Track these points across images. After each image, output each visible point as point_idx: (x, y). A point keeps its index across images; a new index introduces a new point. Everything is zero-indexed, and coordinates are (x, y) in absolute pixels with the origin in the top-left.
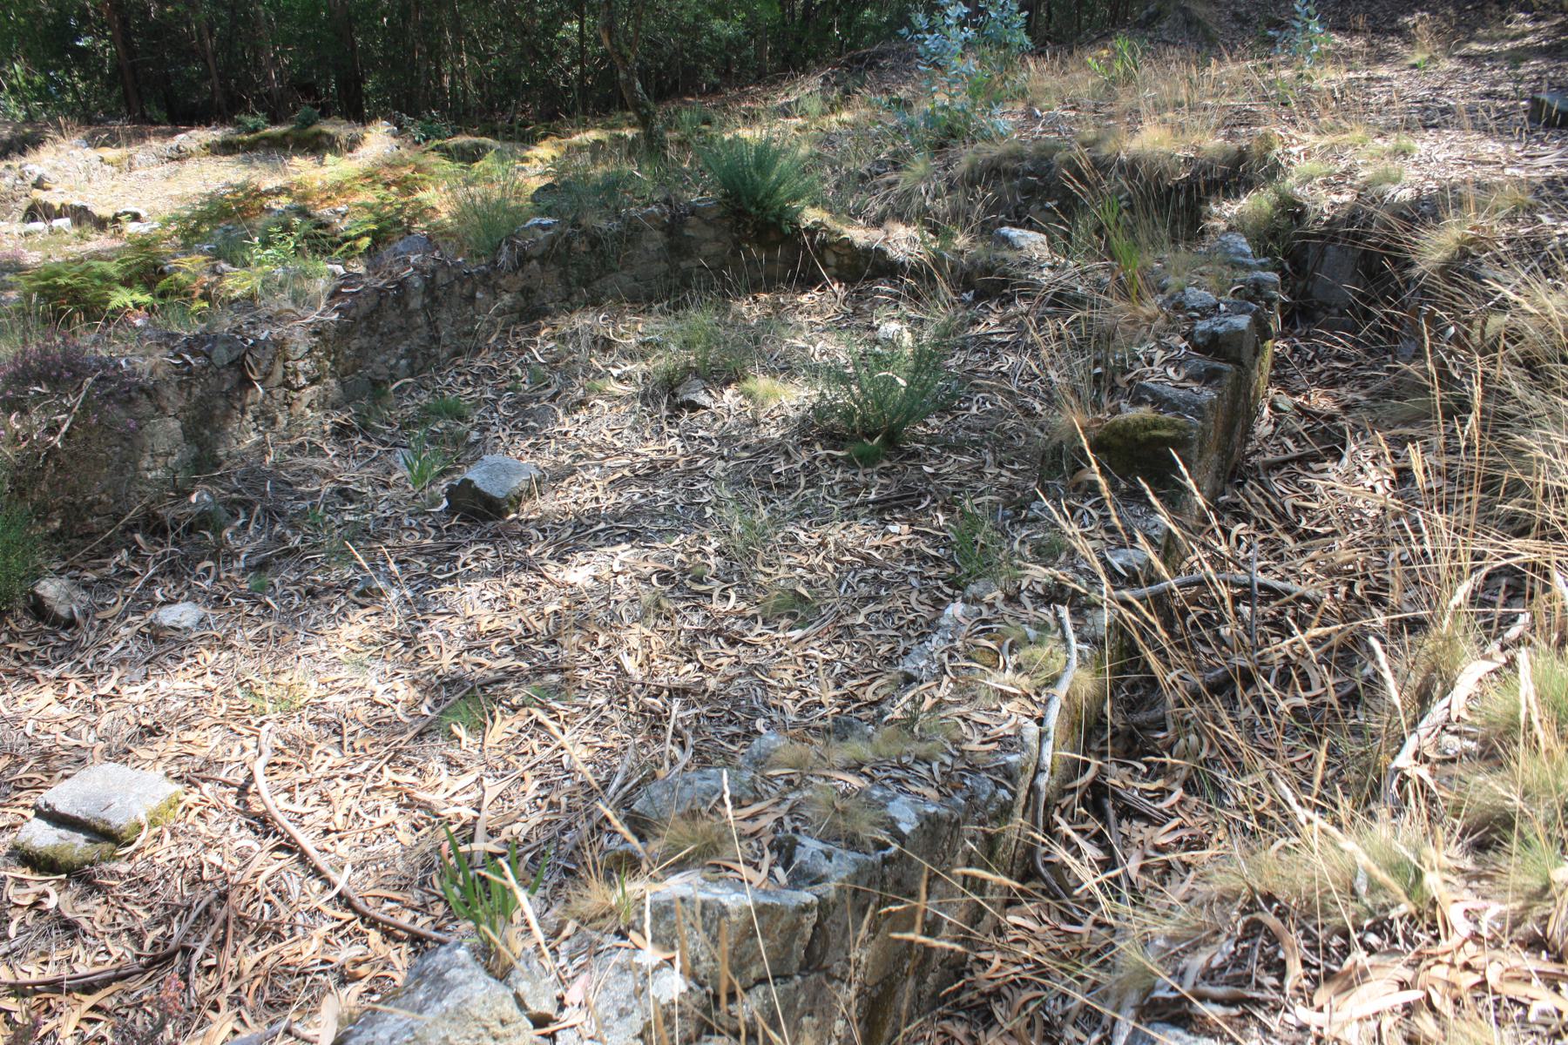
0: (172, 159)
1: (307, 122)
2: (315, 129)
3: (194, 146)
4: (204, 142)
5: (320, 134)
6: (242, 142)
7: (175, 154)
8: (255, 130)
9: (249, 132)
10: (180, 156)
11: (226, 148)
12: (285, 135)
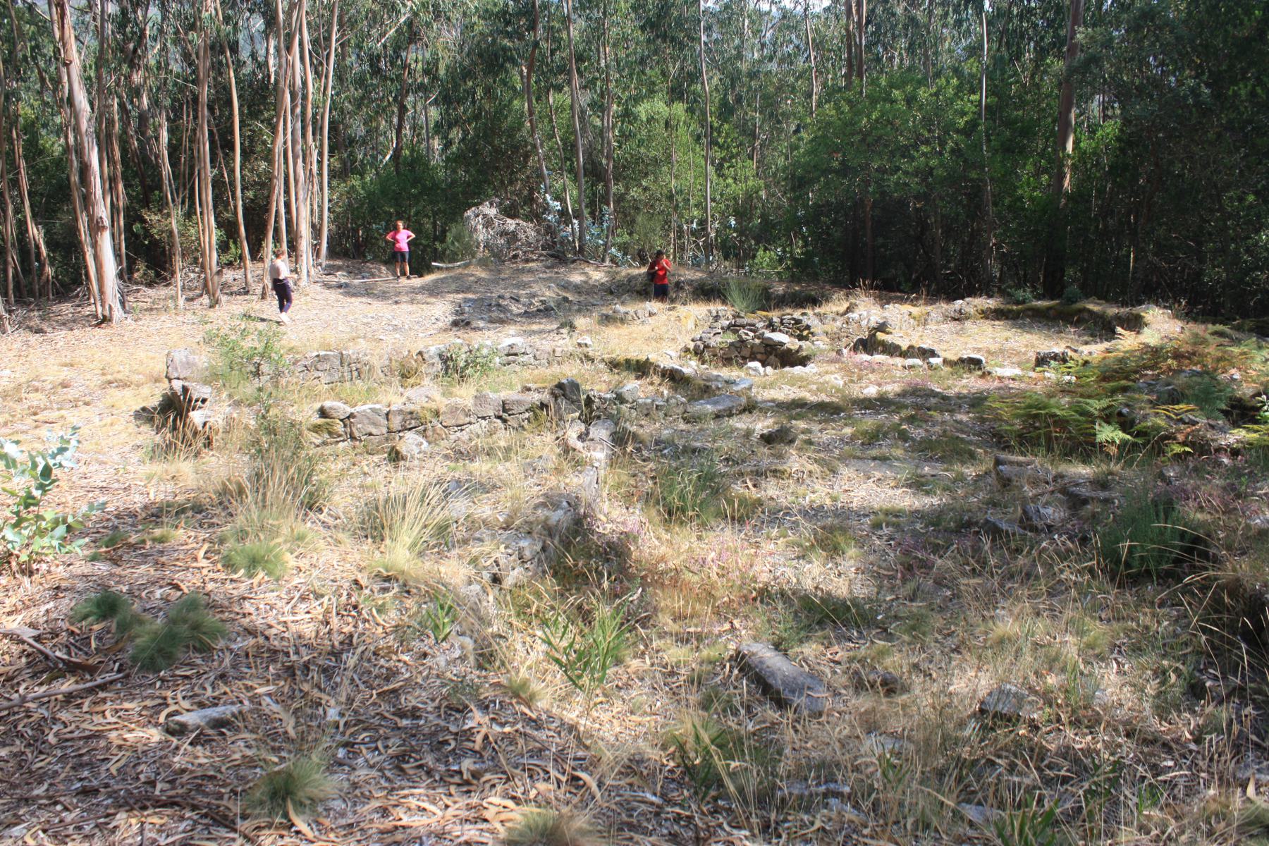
0: (954, 319)
1: (1071, 301)
2: (1079, 305)
3: (972, 311)
4: (979, 308)
5: (1085, 310)
6: (1010, 311)
7: (957, 316)
8: (1023, 302)
9: (1017, 303)
10: (960, 317)
11: (998, 314)
12: (1049, 308)
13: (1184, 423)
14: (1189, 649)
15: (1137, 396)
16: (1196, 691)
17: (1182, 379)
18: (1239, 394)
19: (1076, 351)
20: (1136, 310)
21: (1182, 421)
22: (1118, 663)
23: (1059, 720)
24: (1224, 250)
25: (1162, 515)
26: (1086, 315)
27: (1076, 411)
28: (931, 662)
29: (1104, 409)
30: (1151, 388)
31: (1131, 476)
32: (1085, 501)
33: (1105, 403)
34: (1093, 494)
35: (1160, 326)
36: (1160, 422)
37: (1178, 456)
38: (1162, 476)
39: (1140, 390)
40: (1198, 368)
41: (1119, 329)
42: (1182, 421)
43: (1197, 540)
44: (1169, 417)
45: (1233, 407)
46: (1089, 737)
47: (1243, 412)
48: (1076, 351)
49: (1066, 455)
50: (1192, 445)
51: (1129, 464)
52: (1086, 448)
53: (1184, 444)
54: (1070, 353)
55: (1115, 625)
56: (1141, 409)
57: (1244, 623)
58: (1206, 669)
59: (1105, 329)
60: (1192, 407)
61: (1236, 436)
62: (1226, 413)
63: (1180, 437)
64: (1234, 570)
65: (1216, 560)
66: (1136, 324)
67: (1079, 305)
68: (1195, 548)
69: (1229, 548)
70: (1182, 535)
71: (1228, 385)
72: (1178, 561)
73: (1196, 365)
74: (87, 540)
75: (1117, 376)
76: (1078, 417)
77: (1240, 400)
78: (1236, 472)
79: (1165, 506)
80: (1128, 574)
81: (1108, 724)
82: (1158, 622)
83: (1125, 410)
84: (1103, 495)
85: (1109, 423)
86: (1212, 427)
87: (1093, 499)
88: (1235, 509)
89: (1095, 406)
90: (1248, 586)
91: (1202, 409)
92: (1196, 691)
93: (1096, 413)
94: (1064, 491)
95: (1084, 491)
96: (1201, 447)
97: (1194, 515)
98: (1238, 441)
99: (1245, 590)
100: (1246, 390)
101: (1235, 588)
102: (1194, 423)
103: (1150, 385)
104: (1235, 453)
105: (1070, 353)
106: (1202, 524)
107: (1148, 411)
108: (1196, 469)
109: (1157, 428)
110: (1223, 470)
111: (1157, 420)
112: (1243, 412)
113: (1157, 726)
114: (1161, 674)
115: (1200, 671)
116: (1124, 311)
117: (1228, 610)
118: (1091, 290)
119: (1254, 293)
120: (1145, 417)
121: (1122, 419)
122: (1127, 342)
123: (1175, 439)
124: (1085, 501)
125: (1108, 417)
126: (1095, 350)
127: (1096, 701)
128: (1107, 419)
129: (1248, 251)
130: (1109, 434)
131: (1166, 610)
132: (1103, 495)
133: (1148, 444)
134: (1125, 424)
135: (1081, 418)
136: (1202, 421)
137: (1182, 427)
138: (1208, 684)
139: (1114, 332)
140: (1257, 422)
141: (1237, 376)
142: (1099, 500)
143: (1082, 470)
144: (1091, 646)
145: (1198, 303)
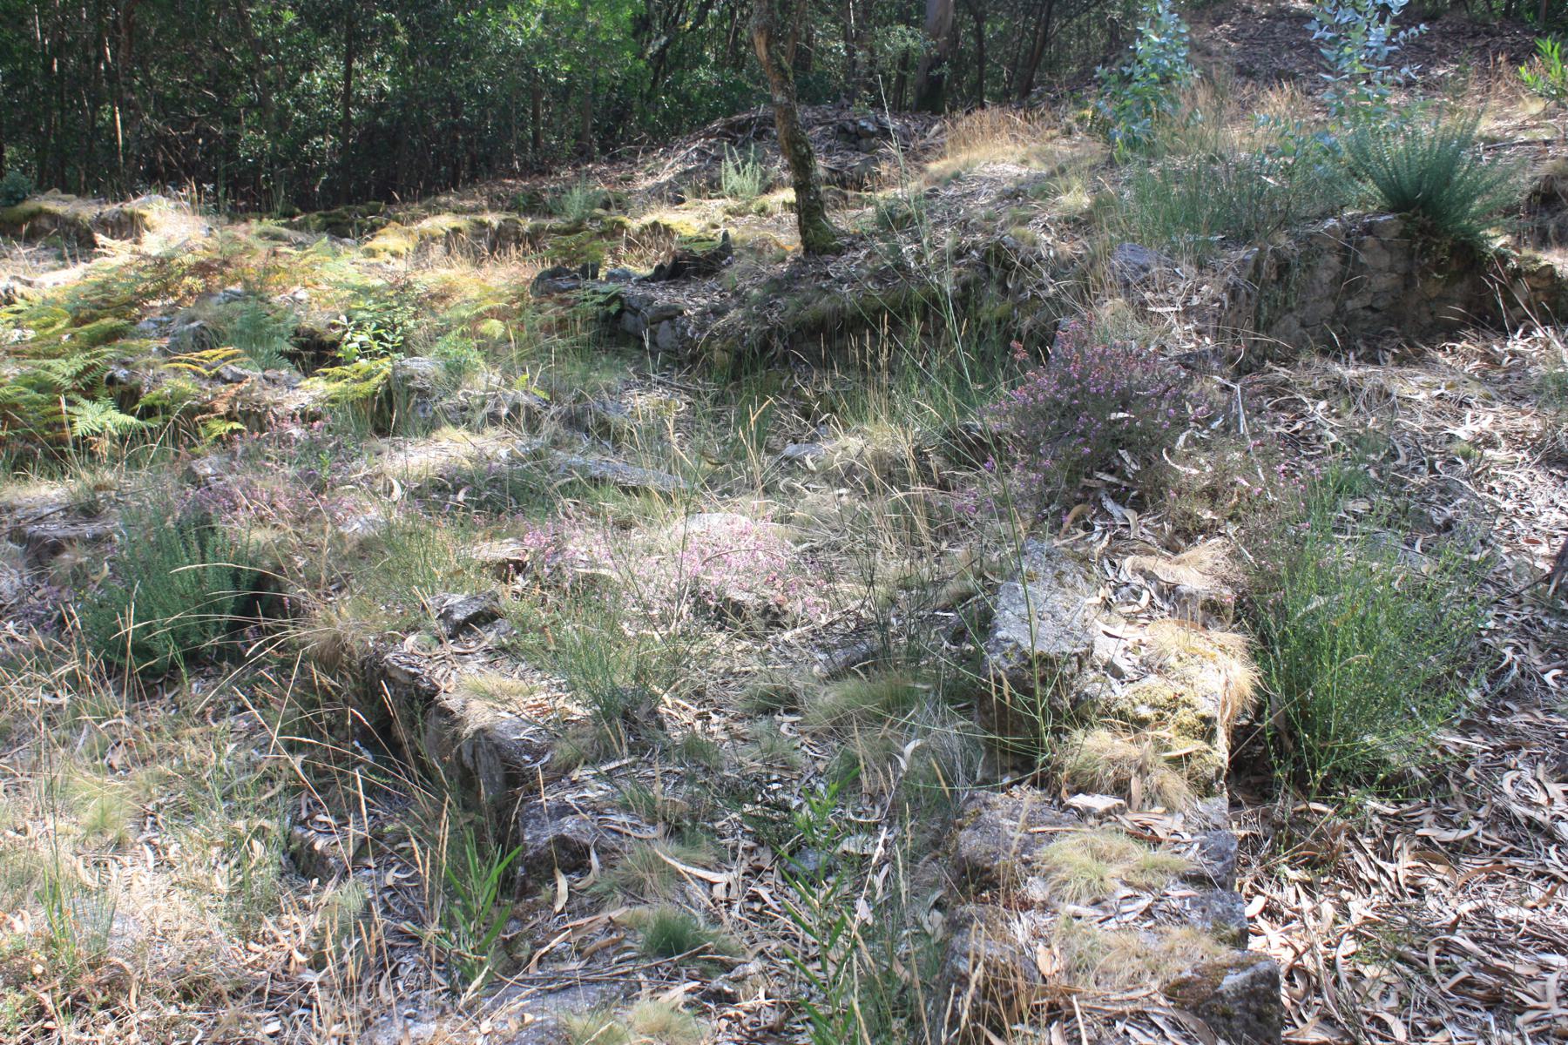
2: (32, 204)
5: (41, 213)
13: (226, 381)
14: (280, 786)
15: (135, 343)
16: (303, 864)
17: (213, 307)
18: (307, 324)
19: (29, 284)
20: (133, 205)
21: (218, 377)
22: (155, 848)
23: (41, 1012)
24: (262, 105)
25: (196, 547)
26: (45, 223)
27: (30, 386)
28: (759, 870)
29: (79, 375)
30: (162, 329)
31: (144, 489)
32: (56, 548)
33: (78, 362)
34: (70, 532)
35: (172, 225)
36: (186, 385)
37: (223, 442)
38: (192, 478)
39: (144, 334)
40: (237, 288)
41: (100, 238)
42: (218, 377)
43: (261, 581)
44: (197, 374)
45: (305, 346)
46: (112, 1026)
47: (315, 352)
48: (29, 284)
49: (14, 468)
50: (246, 417)
51: (134, 463)
52: (52, 450)
53: (229, 417)
54: (20, 288)
55: (139, 774)
56: (148, 366)
57: (356, 719)
58: (311, 817)
59: (77, 241)
60: (231, 350)
61: (313, 390)
62: (292, 357)
63: (222, 408)
64: (329, 622)
65: (297, 611)
66: (128, 227)
67: (32, 204)
68: (261, 595)
69: (314, 583)
70: (236, 577)
71: (288, 311)
72: (234, 628)
73: (233, 282)
74: (534, 989)
75: (105, 318)
76: (32, 394)
77: (312, 333)
78: (313, 447)
79: (201, 528)
80: (148, 674)
81: (143, 984)
82: (217, 749)
83: (121, 373)
84: (88, 530)
85: (94, 399)
86: (274, 382)
87: (70, 540)
88: (317, 511)
89: (63, 370)
90: (356, 645)
91: (252, 354)
92: (303, 864)
93: (68, 384)
94: (17, 536)
95: (55, 529)
96: (255, 418)
97: (252, 534)
98: (315, 400)
99: (351, 654)
100: (315, 319)
101: (332, 658)
102: (239, 379)
103: (160, 323)
104: (308, 417)
105: (20, 288)
106: (264, 550)
107: (163, 368)
108: (248, 456)
109: (178, 396)
110: (293, 450)
111: (174, 381)
112: (315, 352)
113: (233, 957)
114: (233, 845)
115: (303, 823)
116: (110, 209)
117: (330, 698)
118: (56, 178)
119: (321, 169)
120: (157, 380)
121: (117, 390)
122: (116, 254)
123: (212, 410)
124: (56, 548)
125: (89, 387)
126: (59, 280)
127: (115, 944)
128: (90, 393)
129: (299, 105)
130: (96, 418)
131: (228, 722)
132: (88, 530)
133: (169, 426)
134: (126, 398)
135: (39, 397)
136: (253, 373)
137: (222, 388)
138: (319, 845)
139: (95, 245)
140: (336, 362)
141: (302, 295)
142: (85, 542)
143: (43, 493)
144: (99, 829)
145: (236, 190)
